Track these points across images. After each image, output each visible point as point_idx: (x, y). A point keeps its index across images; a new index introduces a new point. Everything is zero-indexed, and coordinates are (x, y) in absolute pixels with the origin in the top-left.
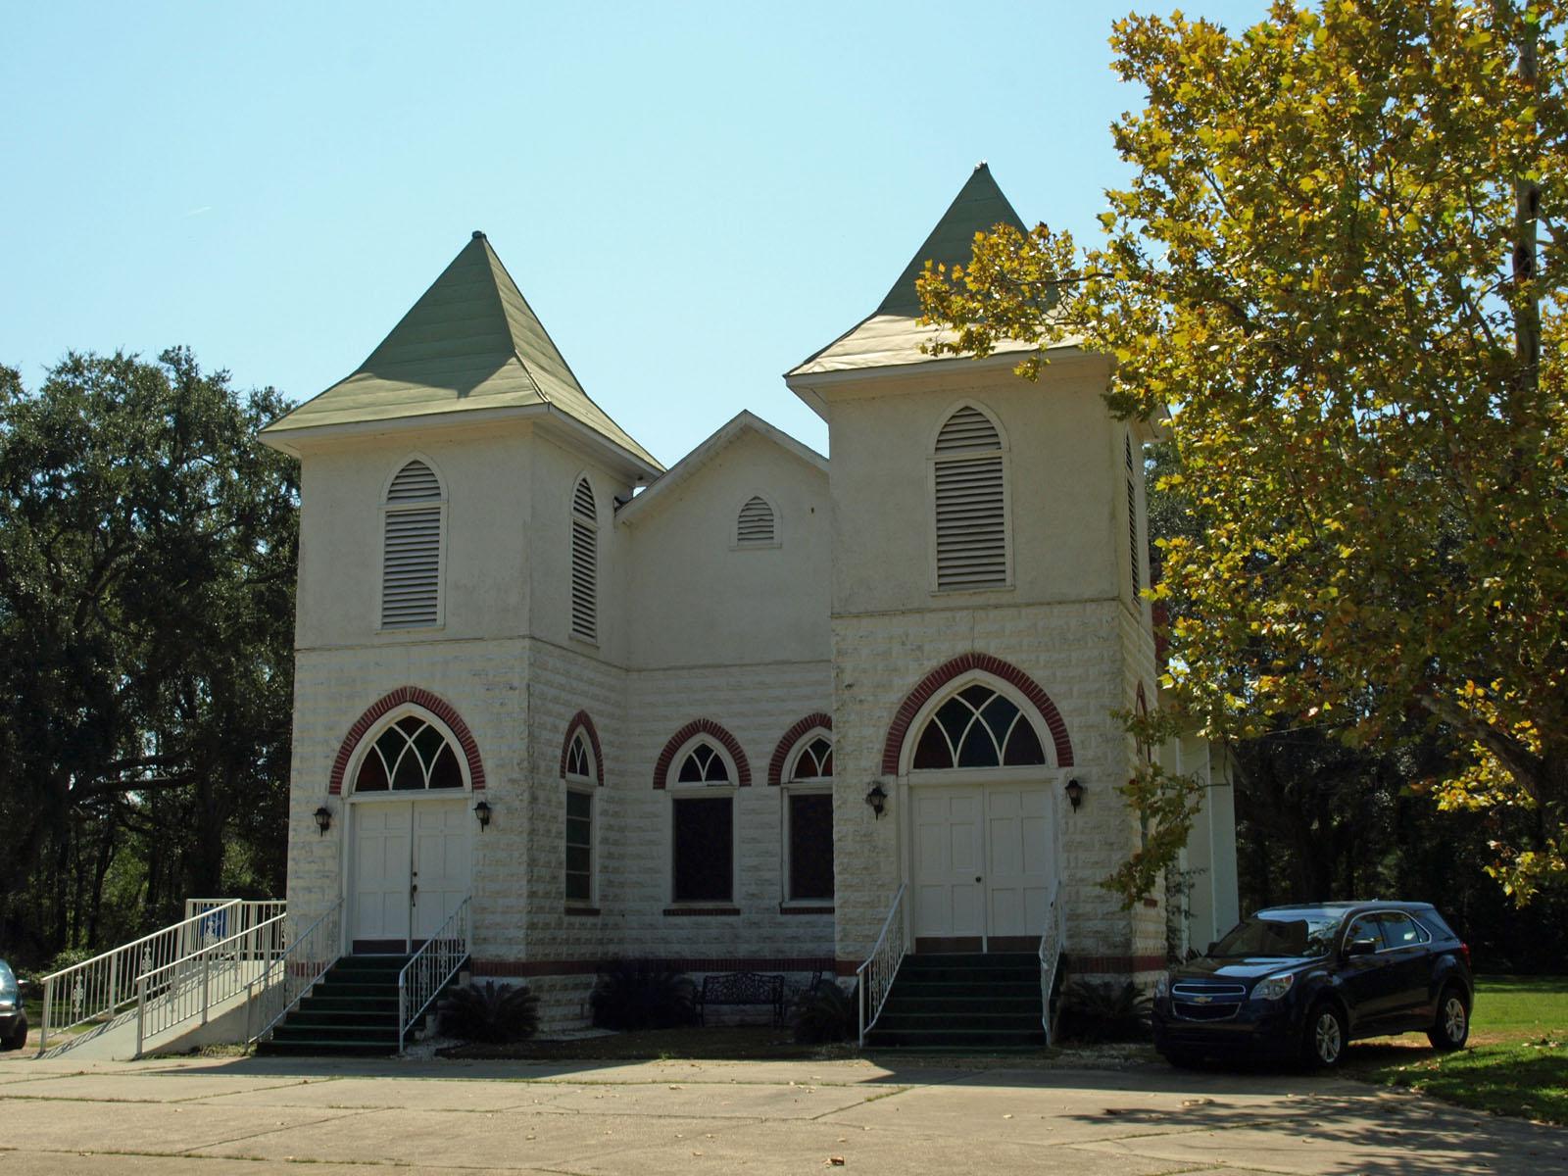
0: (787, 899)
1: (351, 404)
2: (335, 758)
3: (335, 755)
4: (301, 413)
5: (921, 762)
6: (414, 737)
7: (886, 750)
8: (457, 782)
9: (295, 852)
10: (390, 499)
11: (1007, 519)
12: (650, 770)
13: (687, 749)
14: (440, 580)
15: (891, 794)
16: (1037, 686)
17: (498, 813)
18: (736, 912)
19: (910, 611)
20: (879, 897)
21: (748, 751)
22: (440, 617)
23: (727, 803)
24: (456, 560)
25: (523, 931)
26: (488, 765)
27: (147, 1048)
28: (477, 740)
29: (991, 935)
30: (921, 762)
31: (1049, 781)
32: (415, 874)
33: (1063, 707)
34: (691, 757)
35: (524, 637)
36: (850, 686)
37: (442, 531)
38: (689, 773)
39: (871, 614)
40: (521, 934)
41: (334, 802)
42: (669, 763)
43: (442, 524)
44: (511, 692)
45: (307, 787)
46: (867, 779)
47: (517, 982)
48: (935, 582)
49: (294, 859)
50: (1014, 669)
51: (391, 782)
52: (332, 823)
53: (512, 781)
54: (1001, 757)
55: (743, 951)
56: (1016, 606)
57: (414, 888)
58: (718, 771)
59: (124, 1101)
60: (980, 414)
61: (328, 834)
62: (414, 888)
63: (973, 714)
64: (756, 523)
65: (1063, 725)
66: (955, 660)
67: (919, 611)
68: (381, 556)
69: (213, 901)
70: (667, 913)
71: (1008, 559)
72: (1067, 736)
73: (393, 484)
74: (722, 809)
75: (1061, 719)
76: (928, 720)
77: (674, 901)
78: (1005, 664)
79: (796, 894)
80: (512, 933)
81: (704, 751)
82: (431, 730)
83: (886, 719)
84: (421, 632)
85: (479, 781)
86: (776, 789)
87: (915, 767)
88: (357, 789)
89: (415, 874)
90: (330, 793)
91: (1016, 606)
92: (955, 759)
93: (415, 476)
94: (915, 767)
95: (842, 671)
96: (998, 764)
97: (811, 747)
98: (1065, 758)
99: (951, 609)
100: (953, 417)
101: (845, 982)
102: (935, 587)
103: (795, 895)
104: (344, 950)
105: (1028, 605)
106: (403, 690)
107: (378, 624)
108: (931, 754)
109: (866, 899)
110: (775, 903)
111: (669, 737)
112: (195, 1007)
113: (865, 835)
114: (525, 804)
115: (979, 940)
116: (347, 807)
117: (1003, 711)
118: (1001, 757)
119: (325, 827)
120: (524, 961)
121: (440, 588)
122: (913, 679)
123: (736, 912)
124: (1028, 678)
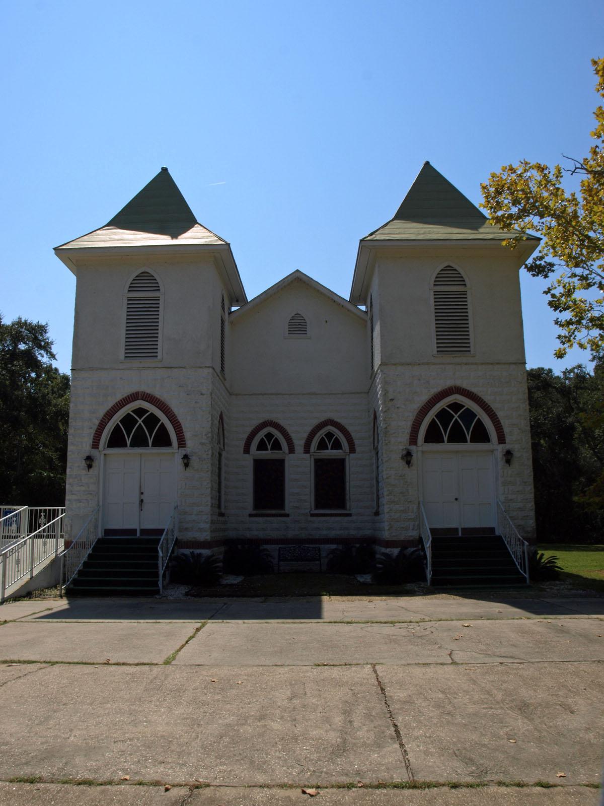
0: (313, 509)
1: (108, 239)
2: (95, 429)
3: (95, 427)
4: (78, 242)
5: (428, 440)
6: (142, 419)
7: (411, 433)
8: (168, 443)
9: (71, 480)
10: (129, 291)
11: (470, 321)
12: (242, 444)
13: (261, 435)
14: (160, 335)
15: (415, 455)
16: (487, 404)
17: (194, 461)
18: (287, 515)
19: (423, 364)
20: (408, 507)
21: (293, 436)
22: (159, 355)
23: (281, 463)
24: (170, 325)
25: (209, 524)
26: (188, 435)
27: (8, 593)
28: (181, 421)
29: (463, 527)
30: (428, 440)
31: (492, 451)
32: (142, 493)
33: (500, 414)
34: (263, 438)
35: (209, 367)
36: (392, 400)
37: (161, 309)
38: (262, 446)
39: (402, 364)
40: (208, 526)
41: (95, 453)
42: (314, 437)
43: (161, 306)
44: (202, 396)
45: (79, 441)
46: (401, 447)
47: (206, 552)
48: (436, 349)
49: (70, 484)
50: (476, 395)
51: (128, 443)
52: (94, 464)
53: (202, 444)
54: (468, 438)
55: (290, 534)
56: (476, 364)
57: (142, 501)
58: (277, 446)
59: (124, 664)
60: (455, 270)
61: (91, 470)
62: (142, 501)
63: (454, 417)
64: (298, 326)
65: (500, 423)
66: (446, 389)
67: (428, 364)
68: (125, 321)
69: (15, 507)
70: (250, 515)
71: (472, 341)
72: (502, 429)
73: (131, 283)
74: (280, 464)
75: (499, 421)
76: (432, 418)
77: (254, 510)
78: (471, 392)
79: (317, 507)
80: (202, 525)
81: (269, 436)
82: (152, 415)
83: (411, 417)
84: (149, 362)
85: (182, 443)
86: (308, 455)
87: (425, 442)
88: (108, 447)
89: (142, 493)
90: (92, 448)
91: (476, 364)
92: (446, 439)
93: (145, 280)
94: (425, 442)
95: (388, 392)
96: (467, 442)
97: (325, 435)
98: (502, 439)
99: (443, 364)
100: (442, 270)
101: (391, 551)
102: (435, 352)
103: (317, 507)
104: (100, 535)
105: (482, 364)
106: (137, 393)
107: (122, 356)
108: (433, 436)
109: (402, 509)
110: (308, 511)
111: (252, 429)
112: (27, 569)
113: (401, 476)
114: (210, 456)
115: (457, 529)
116: (102, 456)
117: (469, 415)
118: (468, 438)
119: (90, 467)
120: (209, 540)
121: (160, 339)
122: (425, 398)
123: (287, 515)
124: (483, 400)
